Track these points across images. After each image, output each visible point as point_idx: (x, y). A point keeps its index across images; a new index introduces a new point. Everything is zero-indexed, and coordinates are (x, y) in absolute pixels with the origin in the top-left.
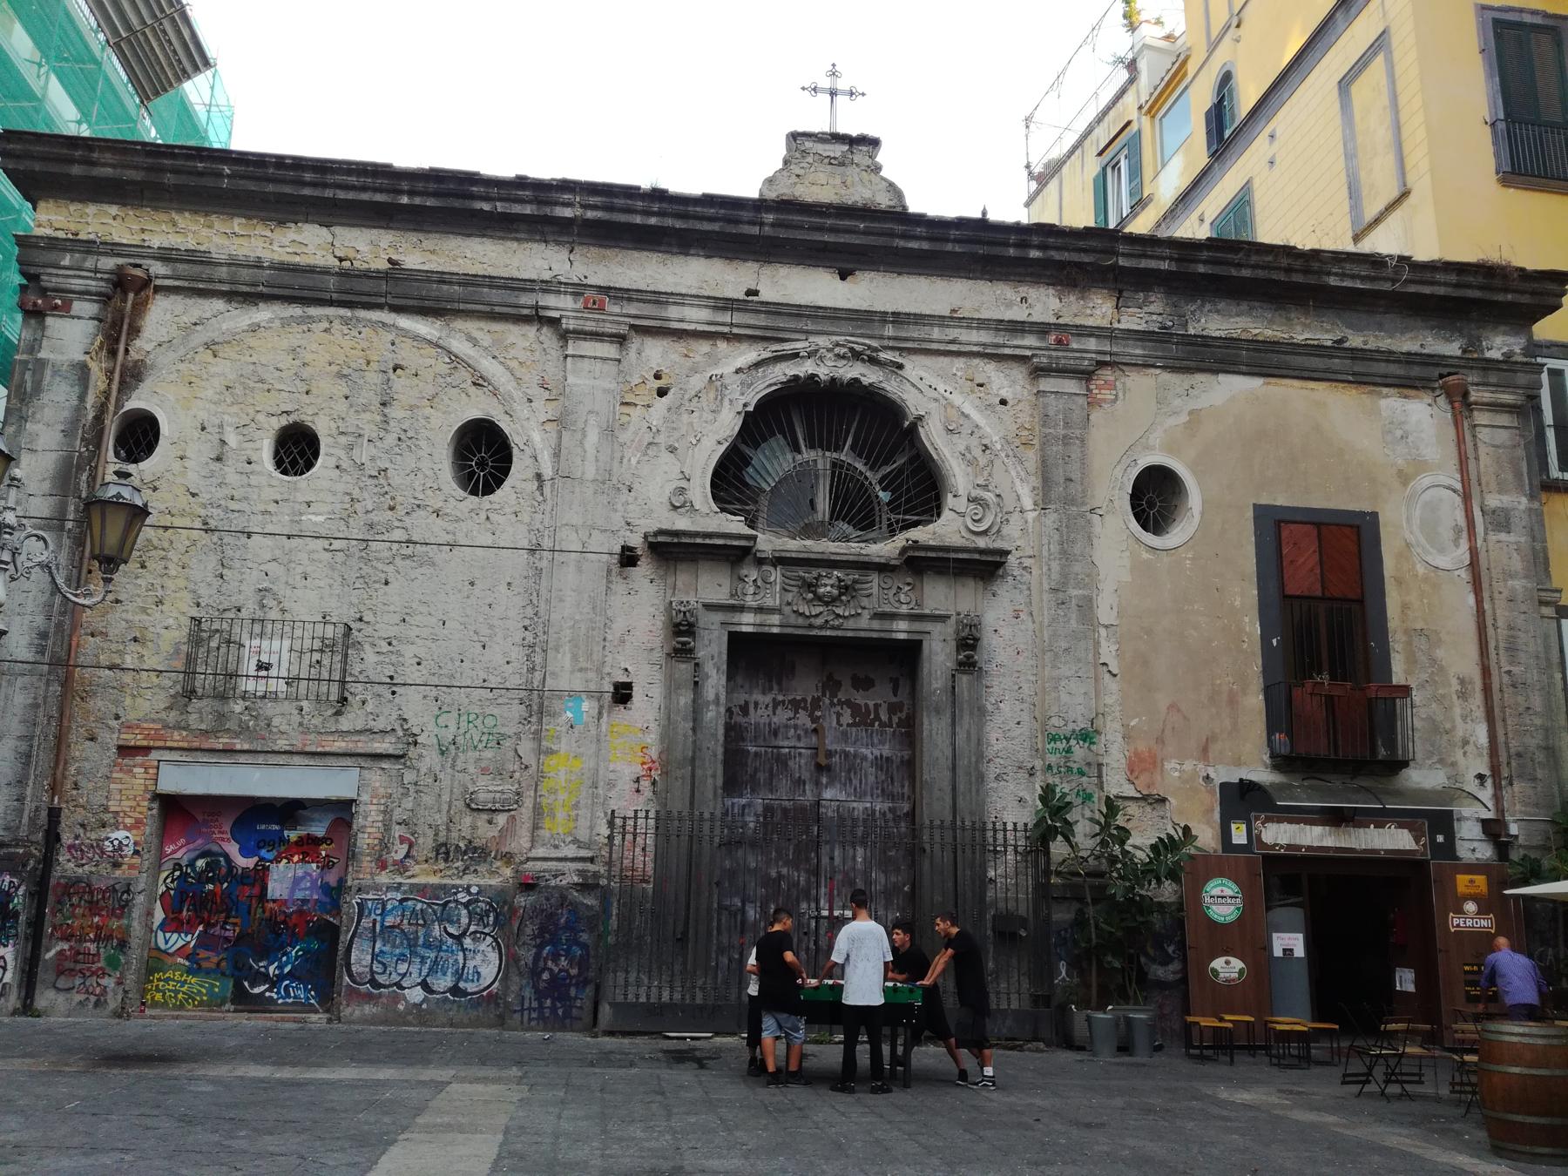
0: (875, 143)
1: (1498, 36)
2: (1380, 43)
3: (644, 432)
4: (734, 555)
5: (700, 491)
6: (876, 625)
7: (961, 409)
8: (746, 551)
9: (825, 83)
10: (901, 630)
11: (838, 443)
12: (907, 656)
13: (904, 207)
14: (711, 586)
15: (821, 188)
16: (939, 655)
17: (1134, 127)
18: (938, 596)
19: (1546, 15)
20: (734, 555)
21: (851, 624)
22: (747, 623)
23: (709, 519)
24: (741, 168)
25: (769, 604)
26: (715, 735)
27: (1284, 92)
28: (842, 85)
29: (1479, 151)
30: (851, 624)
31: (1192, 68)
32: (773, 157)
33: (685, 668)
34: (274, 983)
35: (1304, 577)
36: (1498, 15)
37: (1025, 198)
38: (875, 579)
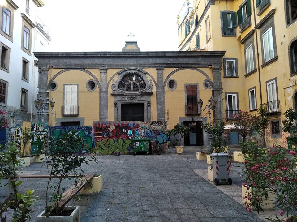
0: (136, 42)
1: (223, 15)
2: (208, 17)
3: (112, 76)
4: (121, 95)
5: (117, 87)
6: (138, 102)
7: (151, 75)
8: (123, 94)
9: (130, 35)
10: (141, 102)
11: (130, 81)
12: (142, 105)
13: (139, 49)
14: (119, 98)
15: (131, 48)
16: (146, 105)
17: (189, 20)
18: (145, 98)
19: (230, 11)
20: (121, 95)
21: (135, 102)
22: (123, 102)
23: (119, 91)
24: (118, 47)
25: (127, 101)
26: (120, 116)
27: (202, 18)
28: (132, 35)
29: (220, 32)
30: (135, 102)
31: (194, 13)
32: (123, 45)
33: (116, 108)
34: (84, 128)
35: (190, 93)
36: (223, 12)
37: (178, 28)
38: (137, 96)
